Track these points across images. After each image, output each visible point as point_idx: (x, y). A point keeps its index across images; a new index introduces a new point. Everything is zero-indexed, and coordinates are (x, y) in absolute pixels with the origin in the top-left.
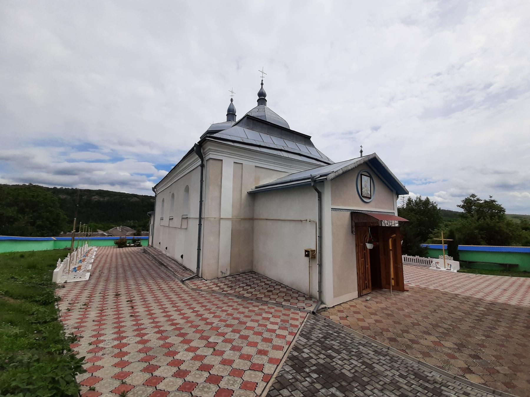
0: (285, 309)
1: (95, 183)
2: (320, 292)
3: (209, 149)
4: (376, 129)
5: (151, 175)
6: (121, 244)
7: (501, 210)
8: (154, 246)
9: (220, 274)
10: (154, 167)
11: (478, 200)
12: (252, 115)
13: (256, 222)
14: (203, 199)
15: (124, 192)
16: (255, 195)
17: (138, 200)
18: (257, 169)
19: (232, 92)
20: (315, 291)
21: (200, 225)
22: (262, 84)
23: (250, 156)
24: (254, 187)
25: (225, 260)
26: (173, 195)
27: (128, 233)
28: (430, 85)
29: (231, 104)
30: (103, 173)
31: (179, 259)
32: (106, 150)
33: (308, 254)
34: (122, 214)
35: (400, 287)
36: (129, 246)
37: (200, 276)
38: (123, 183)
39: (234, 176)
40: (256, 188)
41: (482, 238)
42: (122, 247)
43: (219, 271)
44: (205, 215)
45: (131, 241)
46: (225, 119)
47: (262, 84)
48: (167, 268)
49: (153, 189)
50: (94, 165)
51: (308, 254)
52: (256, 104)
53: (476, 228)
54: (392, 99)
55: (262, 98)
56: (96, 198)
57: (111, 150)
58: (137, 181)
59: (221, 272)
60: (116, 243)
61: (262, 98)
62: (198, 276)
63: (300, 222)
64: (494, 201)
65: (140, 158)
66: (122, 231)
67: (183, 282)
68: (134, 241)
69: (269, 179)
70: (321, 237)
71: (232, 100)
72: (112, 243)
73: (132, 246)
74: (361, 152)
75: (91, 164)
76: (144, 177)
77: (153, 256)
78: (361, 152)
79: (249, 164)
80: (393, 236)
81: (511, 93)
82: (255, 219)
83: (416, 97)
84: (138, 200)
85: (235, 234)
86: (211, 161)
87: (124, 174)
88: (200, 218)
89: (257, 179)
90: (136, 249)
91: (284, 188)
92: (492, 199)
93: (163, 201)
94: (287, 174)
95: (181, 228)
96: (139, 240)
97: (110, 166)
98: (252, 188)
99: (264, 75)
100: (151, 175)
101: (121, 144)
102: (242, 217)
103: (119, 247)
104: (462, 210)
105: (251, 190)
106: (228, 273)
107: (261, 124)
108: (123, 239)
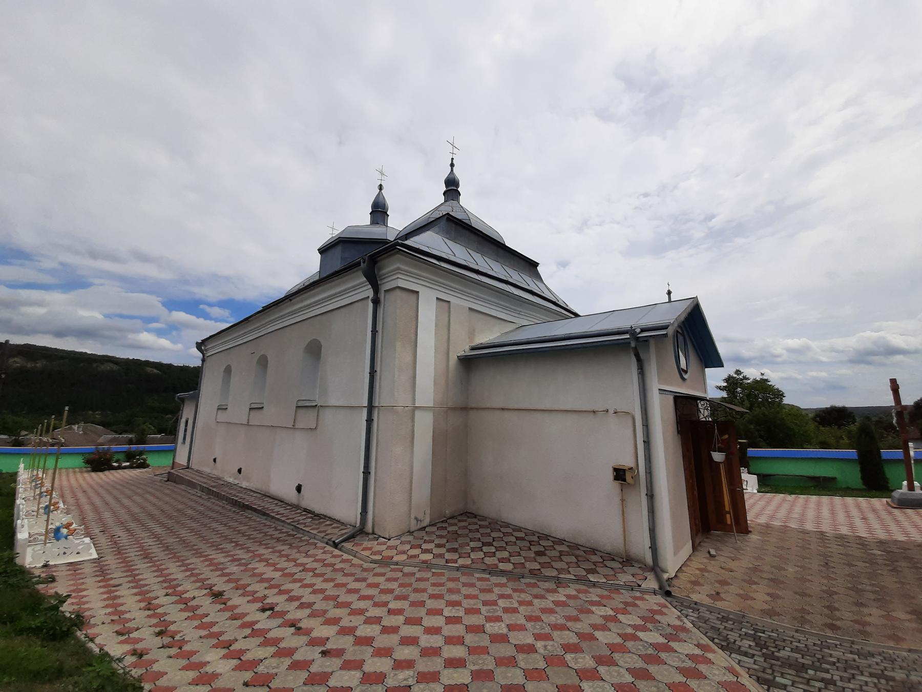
0: (464, 574)
1: (19, 331)
2: (654, 548)
3: (398, 269)
4: (563, 265)
5: (155, 320)
6: (99, 463)
7: (779, 394)
8: (194, 465)
9: (413, 522)
10: (160, 305)
11: (745, 378)
12: (459, 218)
13: (472, 414)
14: (378, 368)
15: (84, 351)
16: (471, 362)
17: (115, 367)
18: (473, 314)
19: (382, 173)
20: (640, 545)
21: (370, 421)
22: (452, 165)
23: (469, 291)
24: (467, 348)
25: (422, 492)
26: (263, 362)
27: (105, 440)
28: (636, 208)
29: (380, 195)
30: (41, 311)
31: (289, 494)
32: (47, 264)
33: (620, 474)
34: (126, 402)
35: (742, 526)
36: (119, 468)
37: (371, 531)
38: (85, 333)
39: (436, 325)
40: (473, 349)
41: (761, 437)
42: (102, 471)
43: (413, 517)
44: (382, 399)
45: (121, 456)
46: (367, 220)
47: (452, 165)
48: (268, 515)
49: (199, 346)
50: (25, 294)
51: (620, 474)
52: (442, 199)
53: (750, 422)
54: (585, 223)
55: (452, 188)
56: (17, 362)
57: (61, 264)
58: (120, 330)
59: (416, 518)
60: (88, 462)
61: (452, 188)
62: (360, 532)
63: (592, 415)
64: (767, 380)
65: (132, 283)
66: (85, 433)
67: (335, 545)
68: (130, 456)
69: (488, 335)
70: (647, 443)
71: (381, 187)
72: (78, 461)
73: (125, 468)
74: (669, 293)
75: (20, 291)
76: (139, 322)
77: (203, 489)
78: (669, 293)
79: (460, 302)
80: (736, 437)
81: (739, 228)
82: (472, 408)
83: (618, 223)
84: (115, 367)
85: (439, 438)
86: (398, 292)
87: (90, 315)
88: (371, 408)
89: (472, 333)
90: (137, 472)
91: (573, 349)
92: (765, 378)
93: (228, 370)
94: (511, 327)
95: (294, 428)
96: (141, 453)
97: (57, 298)
98: (462, 348)
99: (455, 151)
100: (155, 320)
101: (93, 255)
102: (450, 405)
103: (95, 470)
104: (724, 394)
105: (462, 353)
106: (427, 521)
107: (467, 232)
108: (106, 452)
